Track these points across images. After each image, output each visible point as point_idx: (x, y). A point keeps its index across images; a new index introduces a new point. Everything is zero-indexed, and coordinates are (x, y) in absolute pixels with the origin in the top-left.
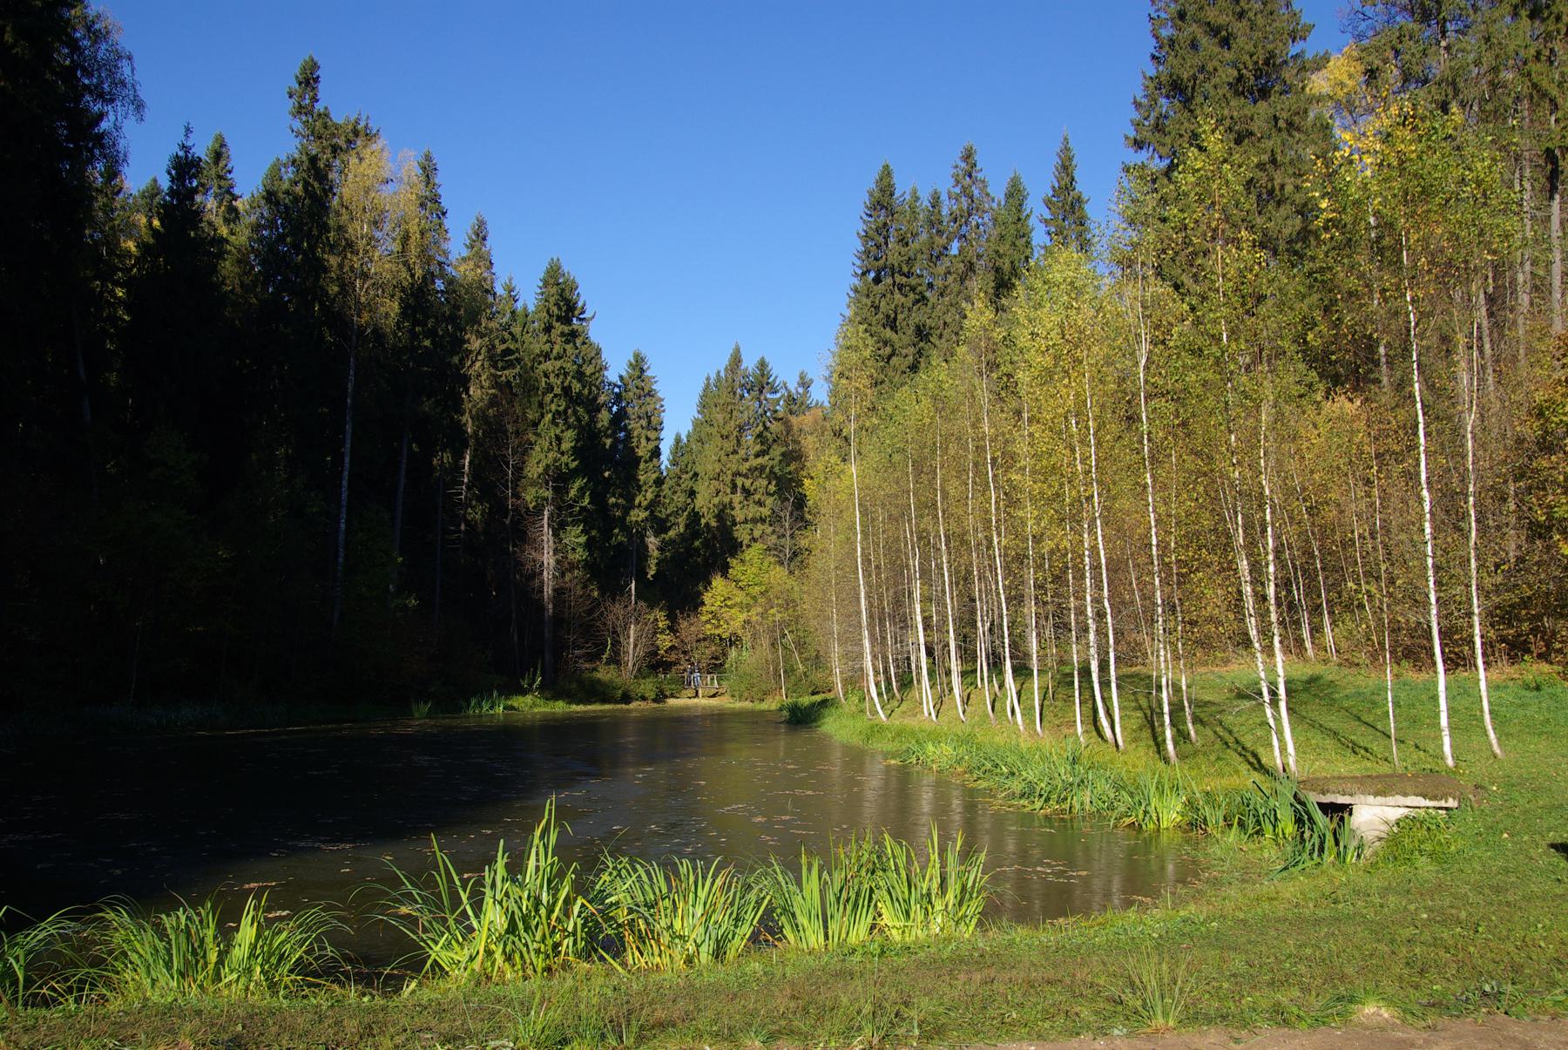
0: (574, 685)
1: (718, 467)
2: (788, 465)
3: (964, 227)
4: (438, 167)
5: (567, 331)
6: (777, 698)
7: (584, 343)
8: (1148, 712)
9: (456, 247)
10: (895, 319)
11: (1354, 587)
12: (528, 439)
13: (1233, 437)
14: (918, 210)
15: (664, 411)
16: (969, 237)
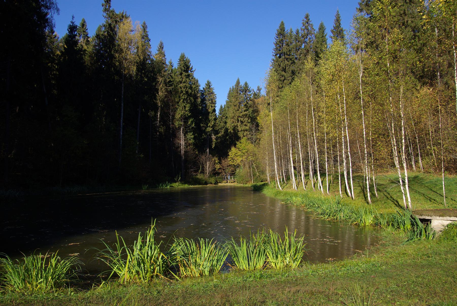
0: (191, 180)
1: (233, 115)
2: (254, 114)
3: (306, 39)
4: (147, 26)
5: (187, 75)
6: (251, 183)
8: (363, 187)
9: (154, 51)
10: (285, 69)
11: (430, 148)
13: (391, 98)
14: (292, 35)
15: (216, 98)
16: (307, 42)
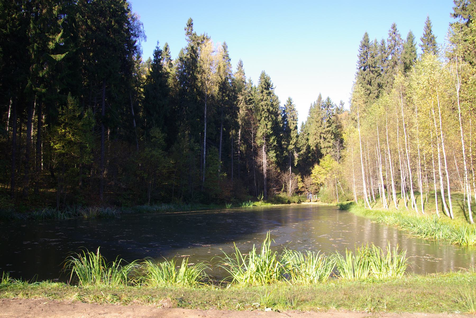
0: (273, 199)
4: (228, 46)
7: (273, 96)
8: (462, 206)
9: (234, 69)
10: (371, 82)
12: (257, 125)
14: (377, 46)
